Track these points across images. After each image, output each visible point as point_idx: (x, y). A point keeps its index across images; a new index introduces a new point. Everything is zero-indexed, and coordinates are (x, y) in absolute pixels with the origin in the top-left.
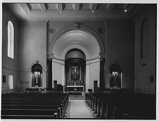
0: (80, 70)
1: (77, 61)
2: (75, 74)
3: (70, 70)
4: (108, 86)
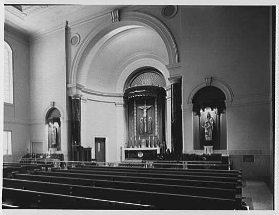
0: (156, 113)
1: (141, 93)
2: (143, 122)
3: (135, 115)
4: (188, 147)
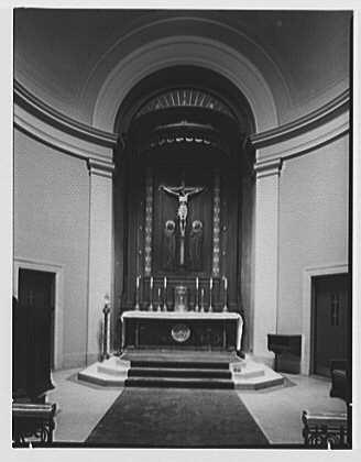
2: (177, 229)
